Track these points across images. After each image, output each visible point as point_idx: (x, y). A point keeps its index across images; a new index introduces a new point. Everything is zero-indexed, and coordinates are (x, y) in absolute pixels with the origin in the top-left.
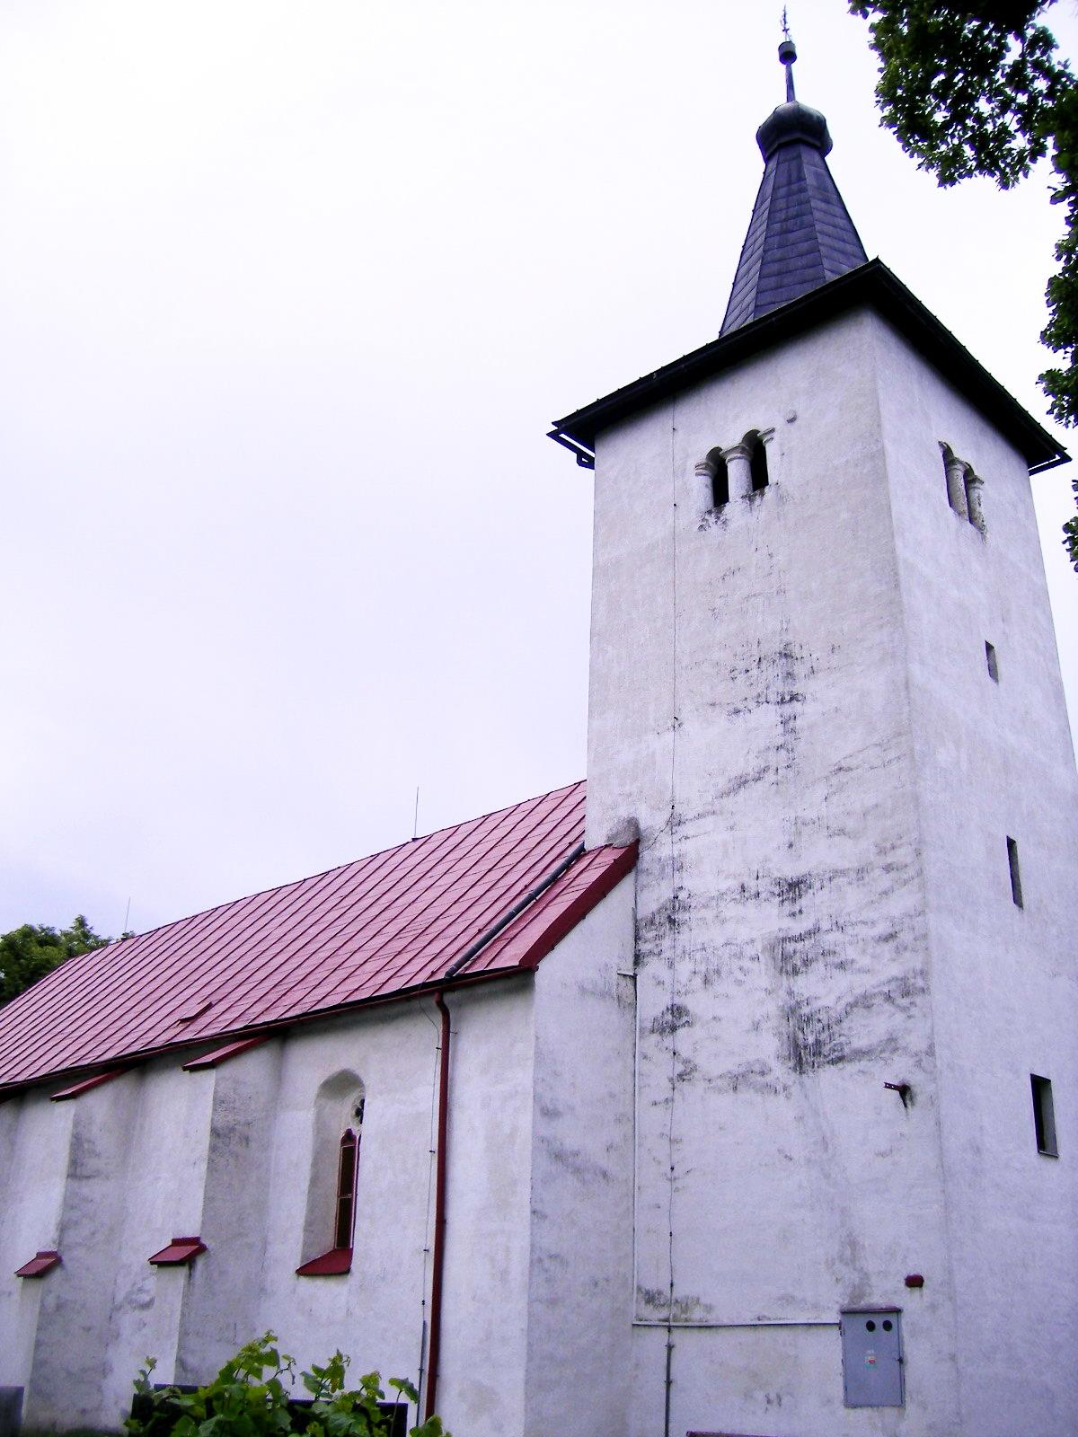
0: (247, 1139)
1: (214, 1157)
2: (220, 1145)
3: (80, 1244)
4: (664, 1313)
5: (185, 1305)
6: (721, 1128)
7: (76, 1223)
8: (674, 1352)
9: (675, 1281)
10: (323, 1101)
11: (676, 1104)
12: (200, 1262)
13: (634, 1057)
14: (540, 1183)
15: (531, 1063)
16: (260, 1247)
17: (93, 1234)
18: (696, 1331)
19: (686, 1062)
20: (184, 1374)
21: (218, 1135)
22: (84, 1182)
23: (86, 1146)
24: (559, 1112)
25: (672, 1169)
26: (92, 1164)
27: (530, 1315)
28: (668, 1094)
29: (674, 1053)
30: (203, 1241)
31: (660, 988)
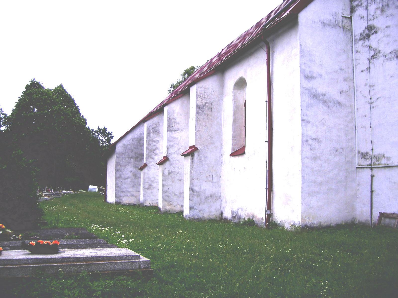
0: (211, 109)
1: (198, 116)
2: (200, 111)
3: (174, 153)
4: (369, 162)
5: (191, 169)
6: (391, 77)
7: (172, 146)
8: (374, 178)
9: (373, 148)
10: (235, 91)
11: (371, 70)
12: (196, 154)
13: (353, 52)
14: (305, 108)
15: (298, 57)
16: (220, 147)
17: (179, 149)
18: (383, 169)
19: (375, 49)
20: (193, 193)
21: (199, 108)
22: (174, 132)
23: (173, 120)
24: (314, 77)
25: (371, 98)
26: (176, 126)
27: (303, 164)
28: (368, 66)
29: (369, 47)
30: (196, 146)
31: (362, 20)
